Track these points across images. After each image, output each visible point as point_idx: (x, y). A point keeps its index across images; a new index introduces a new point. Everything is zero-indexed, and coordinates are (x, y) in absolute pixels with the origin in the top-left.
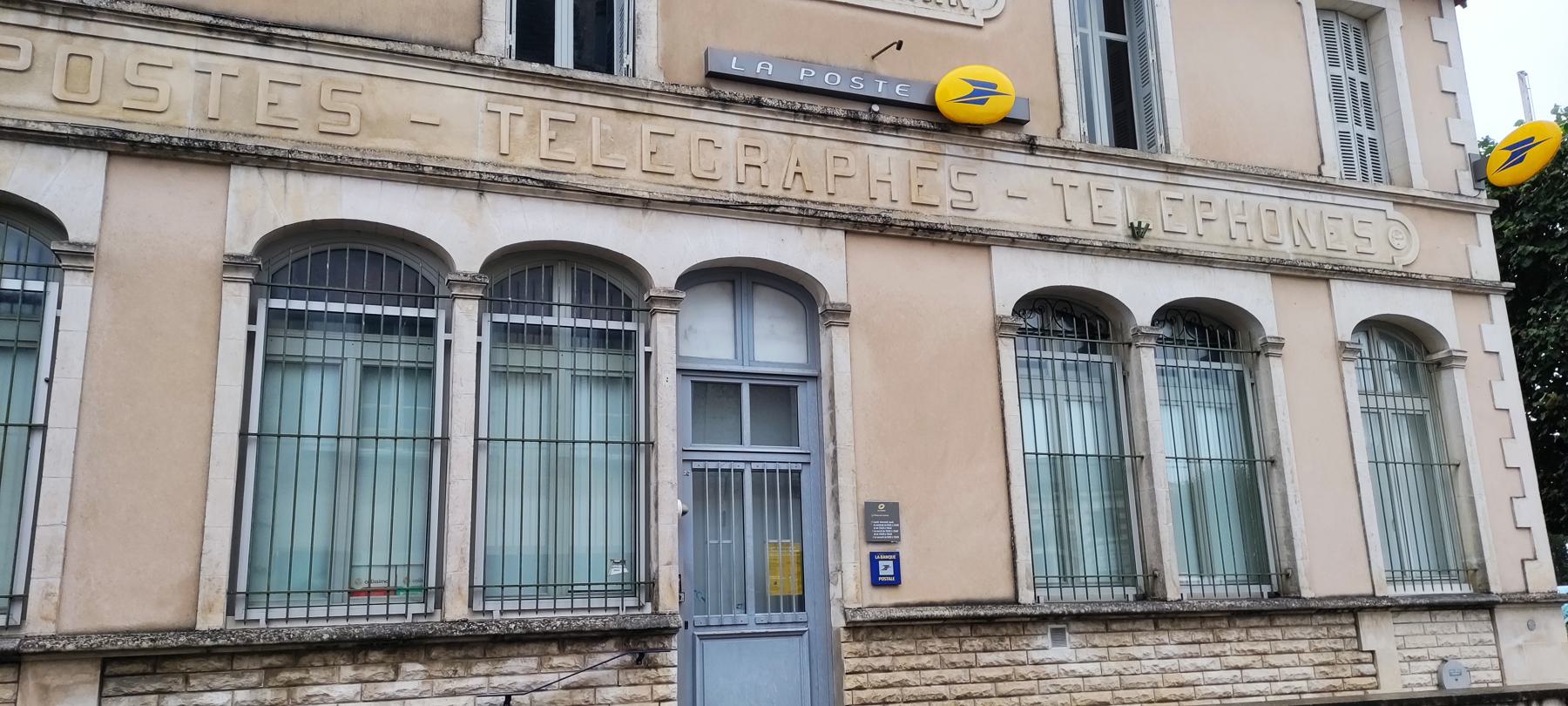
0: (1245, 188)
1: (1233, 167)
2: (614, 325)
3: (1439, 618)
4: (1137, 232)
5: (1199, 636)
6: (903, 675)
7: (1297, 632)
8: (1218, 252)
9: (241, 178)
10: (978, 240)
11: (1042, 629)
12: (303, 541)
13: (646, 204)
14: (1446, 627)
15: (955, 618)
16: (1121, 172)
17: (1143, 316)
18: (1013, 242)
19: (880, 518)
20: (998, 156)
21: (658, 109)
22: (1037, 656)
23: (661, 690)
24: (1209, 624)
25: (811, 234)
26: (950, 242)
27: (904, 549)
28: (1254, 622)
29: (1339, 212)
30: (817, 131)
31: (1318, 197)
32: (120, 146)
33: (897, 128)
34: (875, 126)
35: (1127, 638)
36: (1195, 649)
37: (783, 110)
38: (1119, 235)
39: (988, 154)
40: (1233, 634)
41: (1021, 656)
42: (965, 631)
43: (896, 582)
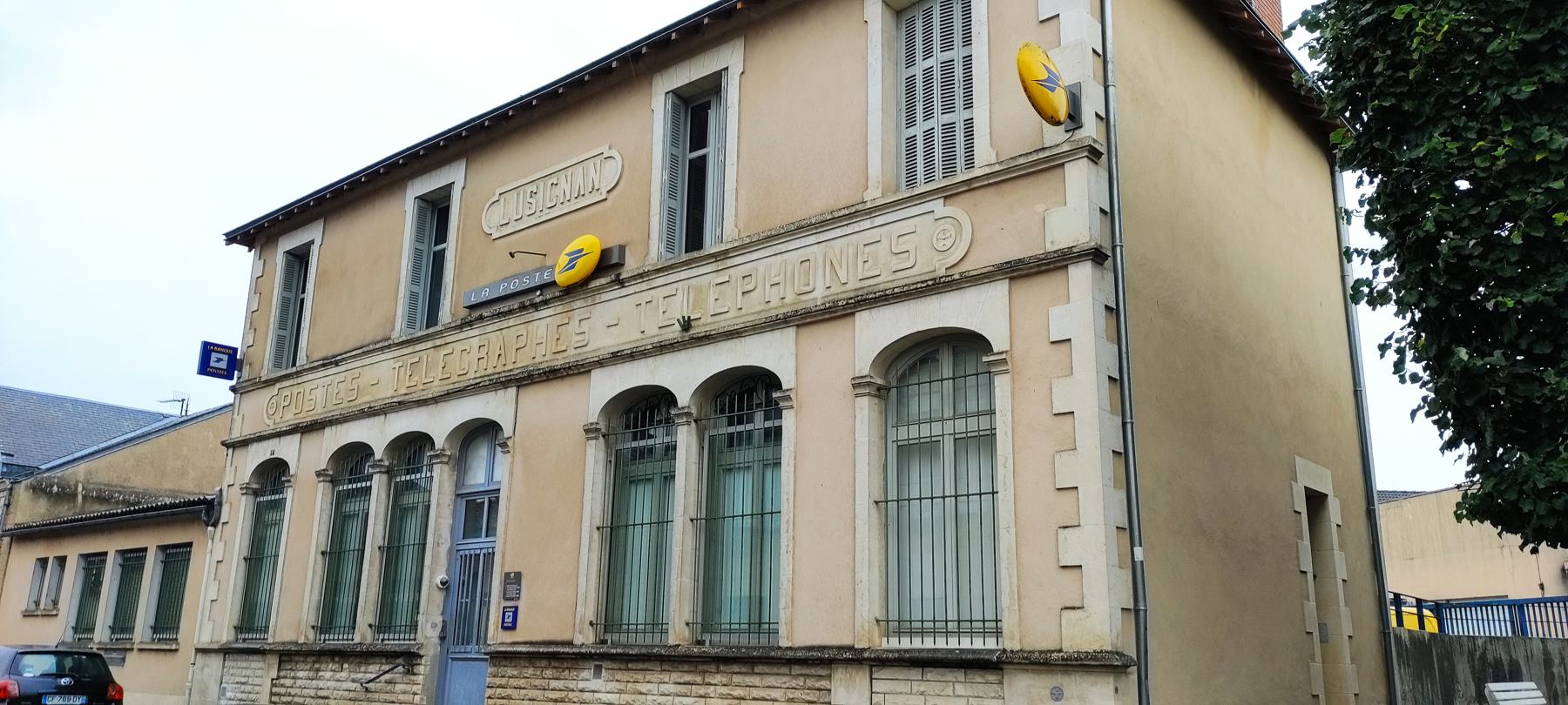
0: (783, 248)
1: (762, 236)
2: (642, 443)
3: (929, 676)
4: (686, 325)
5: (688, 678)
6: (509, 691)
7: (771, 681)
8: (739, 323)
9: (863, 318)
10: (578, 370)
11: (587, 665)
12: (736, 594)
13: (435, 400)
14: (937, 687)
15: (528, 653)
16: (683, 275)
17: (684, 397)
18: (600, 363)
19: (514, 580)
20: (605, 297)
21: (449, 339)
22: (581, 685)
23: (415, 688)
24: (701, 668)
25: (491, 396)
26: (569, 375)
27: (522, 605)
28: (736, 668)
29: (670, 290)
30: (511, 322)
31: (856, 227)
32: (1017, 271)
33: (545, 302)
34: (536, 306)
35: (639, 676)
36: (683, 689)
37: (493, 316)
38: (674, 333)
39: (598, 299)
40: (718, 679)
41: (572, 685)
42: (544, 663)
43: (513, 627)
